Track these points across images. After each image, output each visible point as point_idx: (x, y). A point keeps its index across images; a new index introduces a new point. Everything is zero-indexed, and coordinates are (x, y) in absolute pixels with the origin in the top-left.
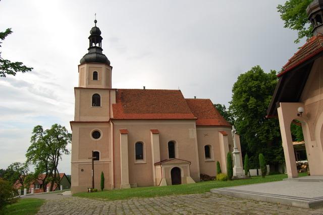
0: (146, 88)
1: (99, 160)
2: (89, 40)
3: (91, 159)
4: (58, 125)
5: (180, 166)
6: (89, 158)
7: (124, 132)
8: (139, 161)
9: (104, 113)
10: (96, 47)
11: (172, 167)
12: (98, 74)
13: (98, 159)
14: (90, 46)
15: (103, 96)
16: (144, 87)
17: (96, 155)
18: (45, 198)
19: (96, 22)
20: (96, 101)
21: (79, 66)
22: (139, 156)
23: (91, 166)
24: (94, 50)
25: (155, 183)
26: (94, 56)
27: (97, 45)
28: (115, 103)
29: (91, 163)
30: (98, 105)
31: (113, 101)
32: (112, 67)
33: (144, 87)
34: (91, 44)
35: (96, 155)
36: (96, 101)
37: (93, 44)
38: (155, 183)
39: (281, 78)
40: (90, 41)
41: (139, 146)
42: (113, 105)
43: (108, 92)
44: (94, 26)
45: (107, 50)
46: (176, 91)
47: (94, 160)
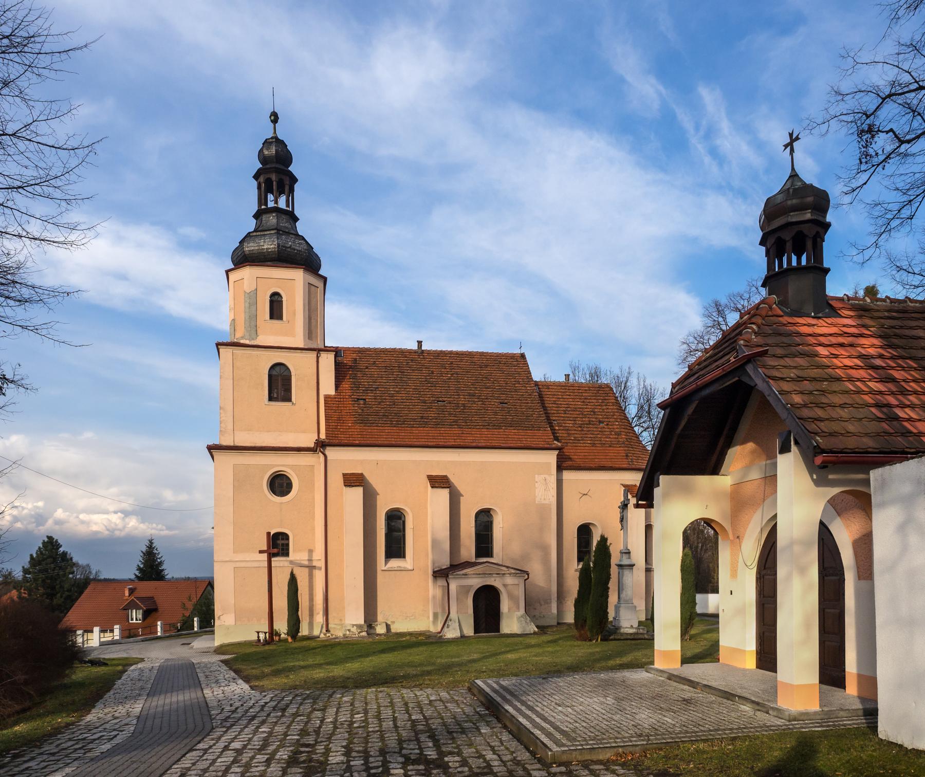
0: (265, 548)
1: (287, 555)
2: (255, 183)
3: (264, 557)
4: (707, 312)
5: (496, 583)
6: (261, 552)
7: (353, 480)
8: (394, 563)
9: (302, 420)
10: (277, 210)
11: (476, 583)
12: (284, 299)
13: (285, 552)
14: (260, 204)
15: (300, 367)
16: (420, 343)
17: (278, 544)
18: (37, 548)
19: (275, 118)
20: (279, 385)
21: (227, 272)
22: (396, 548)
23: (266, 570)
24: (272, 219)
25: (55, 683)
26: (269, 244)
27: (282, 203)
28: (332, 392)
29: (266, 564)
30: (286, 396)
31: (328, 387)
32: (325, 280)
33: (420, 343)
34: (262, 200)
35: (278, 544)
36: (279, 385)
37: (271, 197)
38: (55, 683)
39: (668, 411)
40: (259, 188)
41: (395, 519)
42: (327, 397)
43: (313, 355)
44: (271, 135)
45: (316, 221)
46: (513, 356)
47: (271, 556)
